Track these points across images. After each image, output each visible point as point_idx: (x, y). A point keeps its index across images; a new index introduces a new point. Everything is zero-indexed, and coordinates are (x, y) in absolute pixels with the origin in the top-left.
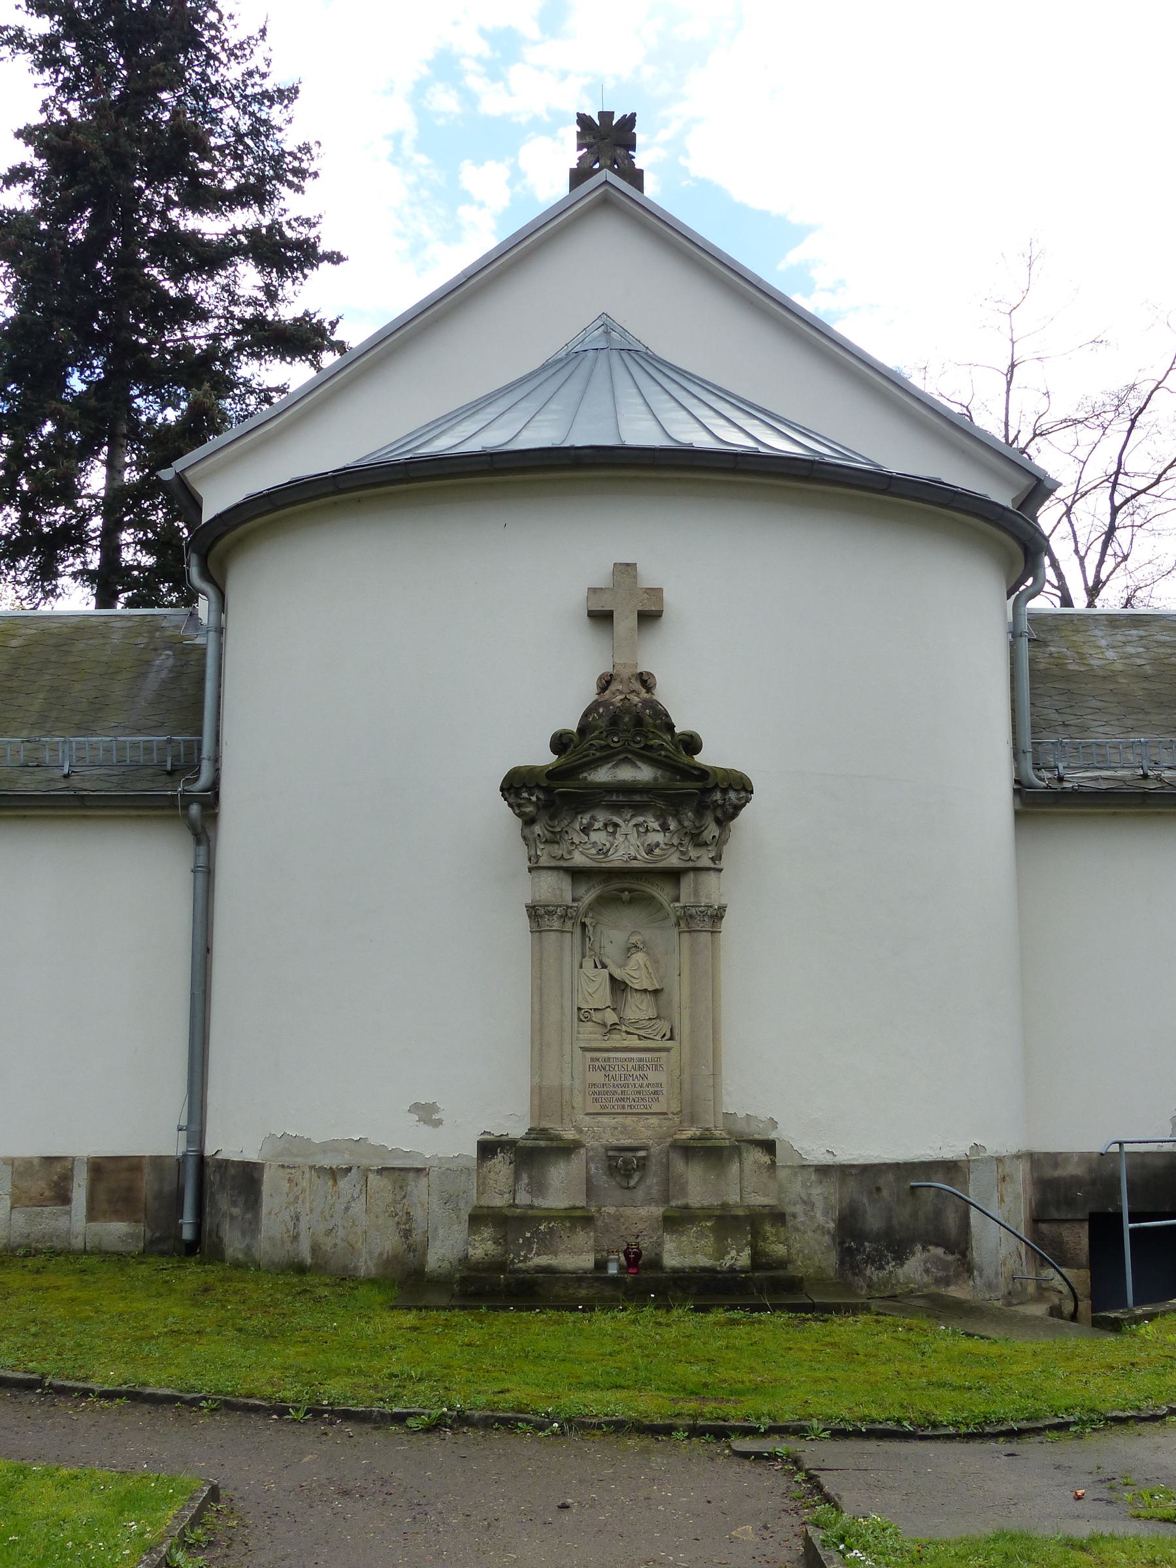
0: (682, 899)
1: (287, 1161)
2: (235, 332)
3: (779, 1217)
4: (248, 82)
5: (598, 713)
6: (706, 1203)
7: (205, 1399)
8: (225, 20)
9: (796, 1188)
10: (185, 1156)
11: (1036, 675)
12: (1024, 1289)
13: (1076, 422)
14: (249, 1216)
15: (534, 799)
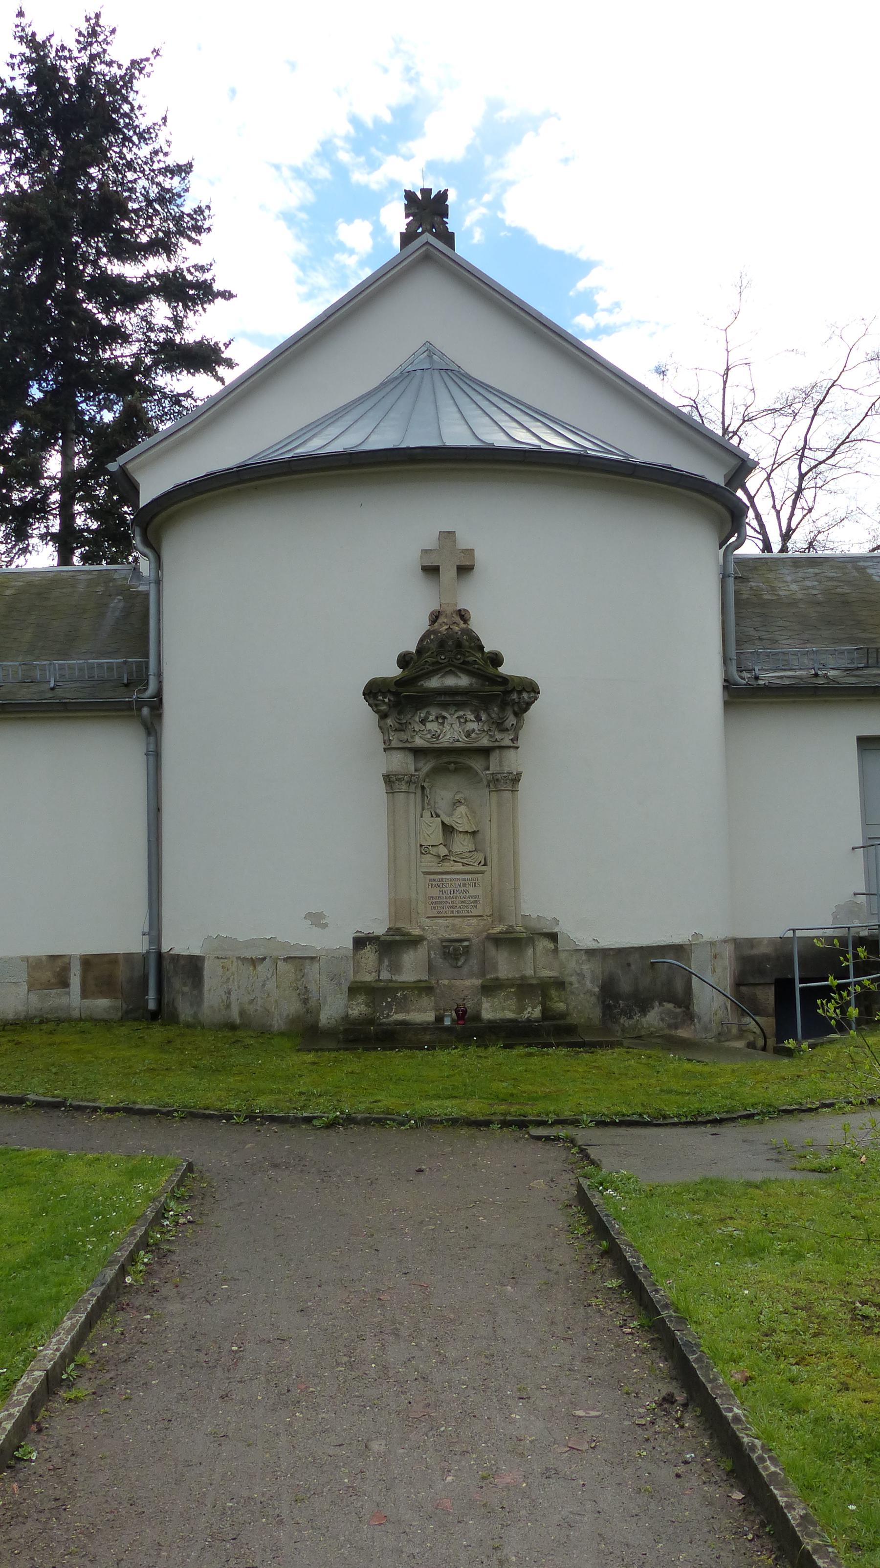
0: (491, 768)
1: (220, 954)
2: (152, 352)
3: (560, 984)
4: (155, 159)
5: (430, 639)
6: (510, 976)
7: (176, 1111)
8: (137, 112)
9: (572, 965)
10: (148, 952)
11: (738, 603)
12: (729, 1031)
13: (775, 411)
14: (195, 992)
15: (386, 700)
